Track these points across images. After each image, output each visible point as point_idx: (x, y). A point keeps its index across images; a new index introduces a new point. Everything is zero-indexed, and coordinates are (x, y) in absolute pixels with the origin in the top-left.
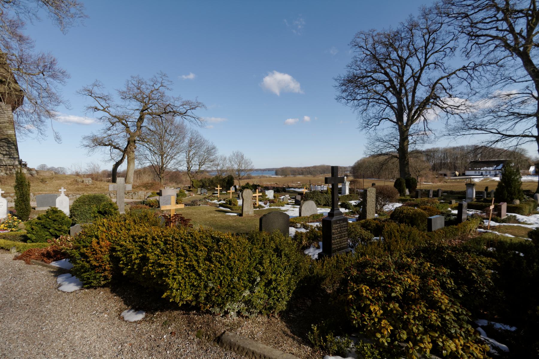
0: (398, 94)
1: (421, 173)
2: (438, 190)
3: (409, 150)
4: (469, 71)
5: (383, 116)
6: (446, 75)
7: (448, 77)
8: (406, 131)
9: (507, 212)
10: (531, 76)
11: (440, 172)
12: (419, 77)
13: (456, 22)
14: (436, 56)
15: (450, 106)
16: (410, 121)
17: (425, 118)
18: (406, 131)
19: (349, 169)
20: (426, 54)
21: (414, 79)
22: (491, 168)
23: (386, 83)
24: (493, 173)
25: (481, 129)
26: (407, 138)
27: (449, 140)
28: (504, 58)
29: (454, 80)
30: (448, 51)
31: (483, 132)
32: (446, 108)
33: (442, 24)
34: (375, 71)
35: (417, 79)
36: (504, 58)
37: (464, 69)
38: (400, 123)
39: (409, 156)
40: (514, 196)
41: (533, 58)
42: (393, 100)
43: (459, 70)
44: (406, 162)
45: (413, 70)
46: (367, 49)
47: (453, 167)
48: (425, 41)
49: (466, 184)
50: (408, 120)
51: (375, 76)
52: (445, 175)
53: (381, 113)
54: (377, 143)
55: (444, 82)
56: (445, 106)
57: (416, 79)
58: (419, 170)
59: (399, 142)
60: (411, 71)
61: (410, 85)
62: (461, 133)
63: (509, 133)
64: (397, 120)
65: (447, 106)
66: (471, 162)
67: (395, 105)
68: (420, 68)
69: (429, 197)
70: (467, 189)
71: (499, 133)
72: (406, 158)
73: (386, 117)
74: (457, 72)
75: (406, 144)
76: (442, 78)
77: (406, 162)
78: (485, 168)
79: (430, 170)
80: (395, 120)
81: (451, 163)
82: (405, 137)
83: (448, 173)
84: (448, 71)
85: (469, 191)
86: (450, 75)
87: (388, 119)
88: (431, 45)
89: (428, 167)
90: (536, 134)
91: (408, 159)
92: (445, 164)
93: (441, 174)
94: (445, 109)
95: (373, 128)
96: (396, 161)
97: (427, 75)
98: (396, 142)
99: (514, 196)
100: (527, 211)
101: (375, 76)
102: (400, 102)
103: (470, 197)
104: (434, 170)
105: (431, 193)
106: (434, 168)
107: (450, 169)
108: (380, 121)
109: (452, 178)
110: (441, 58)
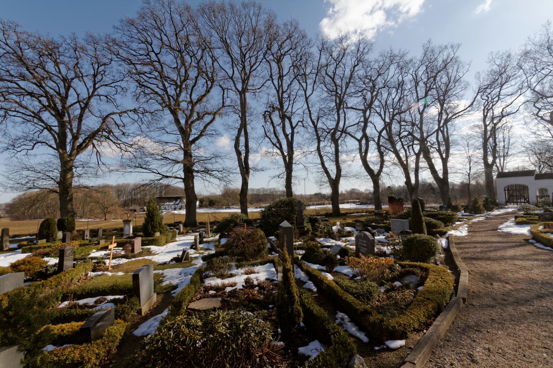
0: (59, 115)
1: (110, 209)
2: (98, 230)
3: (74, 184)
4: (140, 115)
5: (39, 140)
6: (119, 111)
7: (120, 114)
8: (70, 161)
9: (142, 246)
10: (180, 131)
11: (131, 208)
12: (87, 105)
13: (127, 66)
14: (107, 90)
15: (124, 143)
16: (75, 151)
17: (97, 151)
18: (70, 161)
19: (4, 207)
20: (95, 84)
21: (80, 105)
22: (172, 203)
23: (42, 99)
24: (173, 207)
25: (146, 169)
26: (71, 169)
27: (118, 176)
28: (321, 157)
29: (126, 119)
30: (119, 90)
31: (148, 171)
32: (119, 144)
33: (111, 60)
34: (23, 77)
35: (85, 106)
36: (321, 157)
37: (135, 111)
38: (61, 151)
39: (73, 190)
40: (156, 229)
41: (252, 140)
42: (53, 122)
43: (131, 111)
44: (68, 198)
45: (78, 95)
46: (7, 44)
47: (142, 202)
48: (94, 70)
49: (123, 221)
50: (73, 149)
51: (22, 84)
52: (135, 211)
53: (37, 134)
54: (25, 173)
55: (116, 117)
56: (120, 142)
57: (83, 106)
58: (107, 206)
59: (61, 174)
60: (76, 96)
61: (76, 111)
62: (129, 170)
63: (168, 174)
64: (57, 146)
65: (120, 142)
66: (157, 198)
67: (56, 129)
68: (87, 96)
69: (83, 239)
70: (124, 226)
71: (159, 173)
72: (68, 193)
73: (44, 141)
74: (129, 113)
75: (69, 176)
76: (113, 113)
77: (68, 198)
78: (168, 203)
79: (119, 206)
80: (55, 146)
81: (140, 199)
82: (68, 167)
83: (137, 208)
84: (121, 109)
85: (127, 227)
86: (121, 113)
87: (46, 143)
88: (99, 77)
89: (117, 203)
90: (183, 177)
91: (72, 195)
92: (135, 199)
93: (131, 210)
94: (118, 146)
95: (24, 152)
96: (56, 196)
97: (98, 106)
98: (56, 174)
99: (156, 229)
100: (164, 241)
101: (22, 84)
102: (62, 125)
103: (127, 233)
104: (125, 206)
105: (87, 233)
106: (125, 204)
107: (140, 205)
108: (35, 145)
109: (141, 213)
110: (113, 94)
